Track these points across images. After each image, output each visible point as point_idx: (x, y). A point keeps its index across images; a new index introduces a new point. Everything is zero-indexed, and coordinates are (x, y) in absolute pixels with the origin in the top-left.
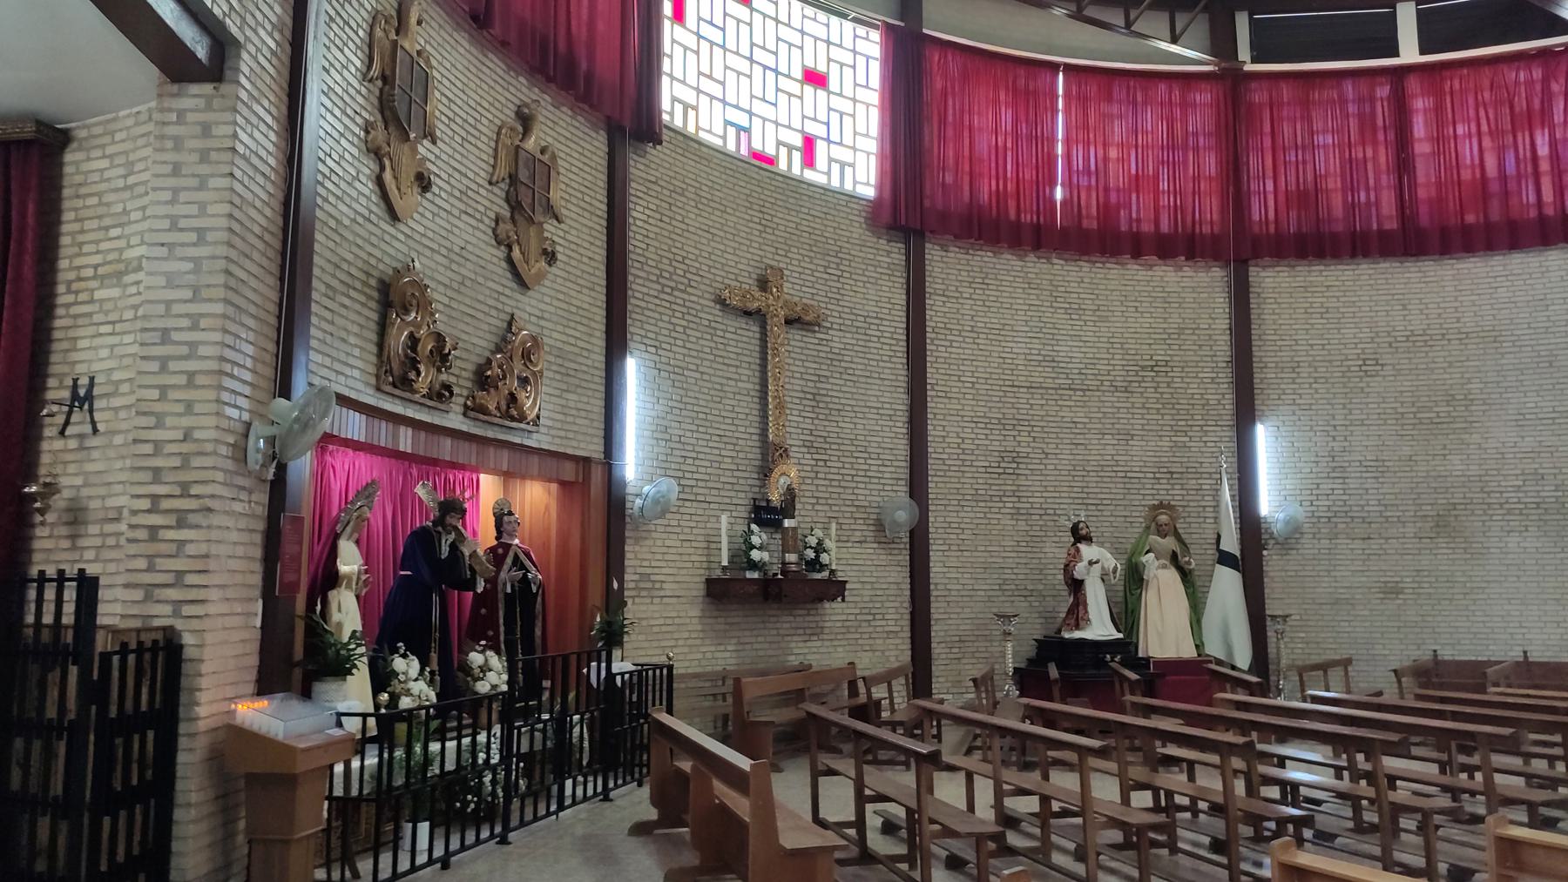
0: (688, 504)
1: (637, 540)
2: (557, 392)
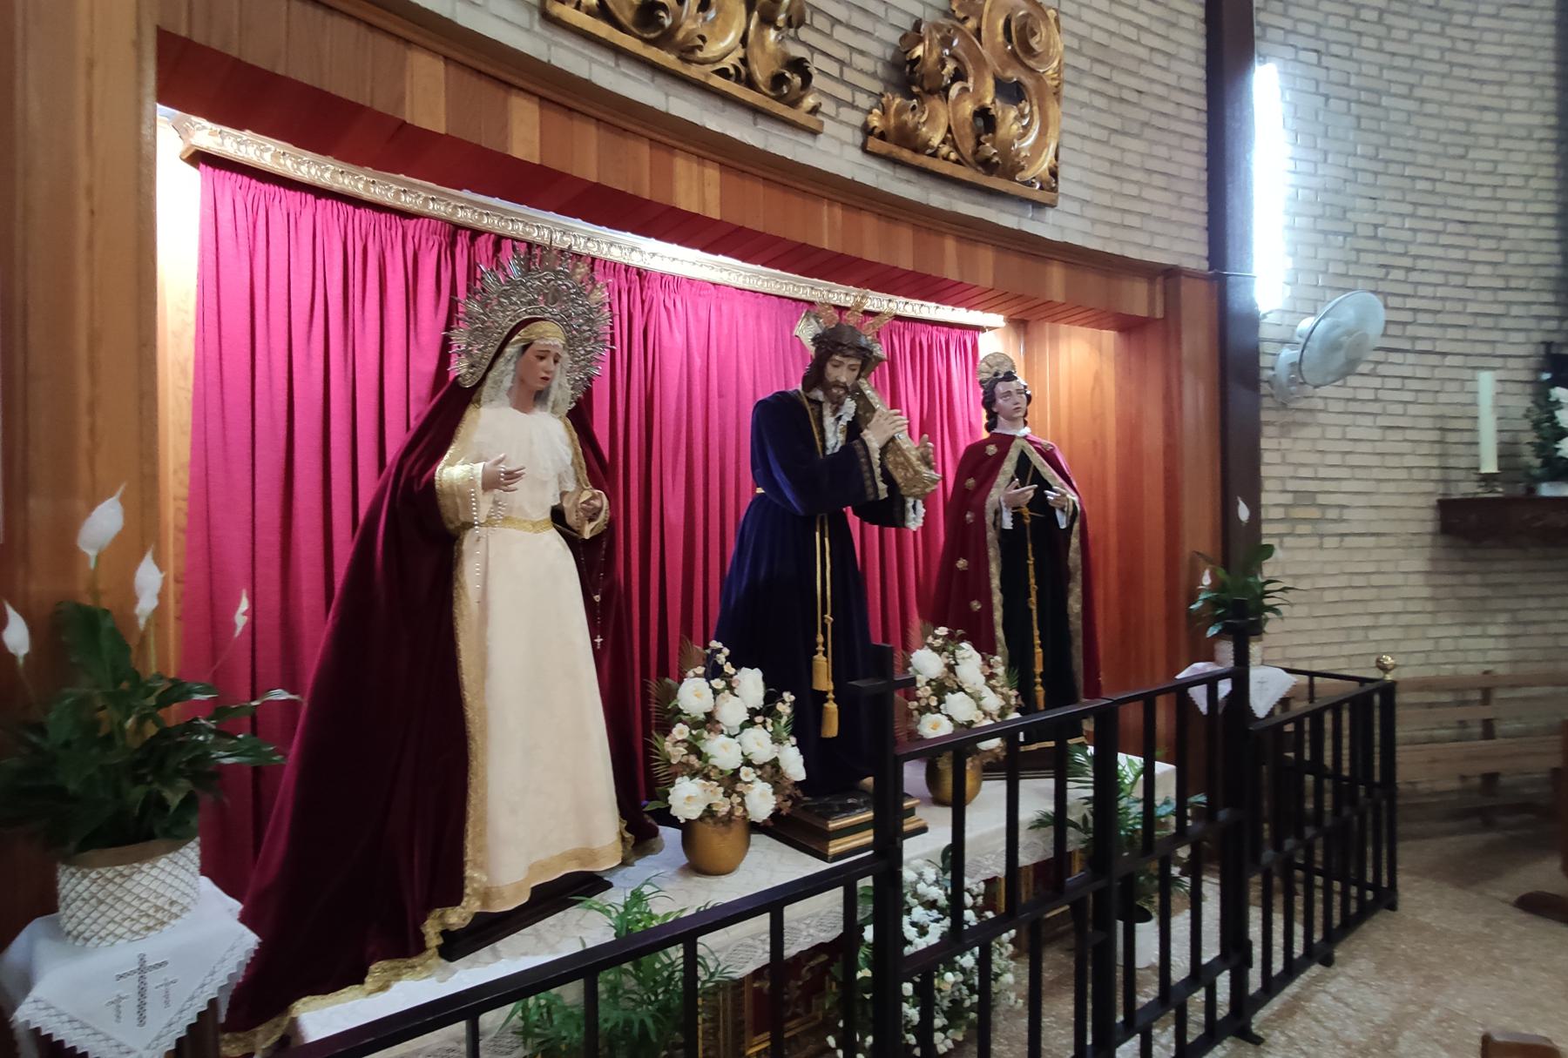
0: (1394, 357)
1: (1285, 429)
2: (1100, 134)
